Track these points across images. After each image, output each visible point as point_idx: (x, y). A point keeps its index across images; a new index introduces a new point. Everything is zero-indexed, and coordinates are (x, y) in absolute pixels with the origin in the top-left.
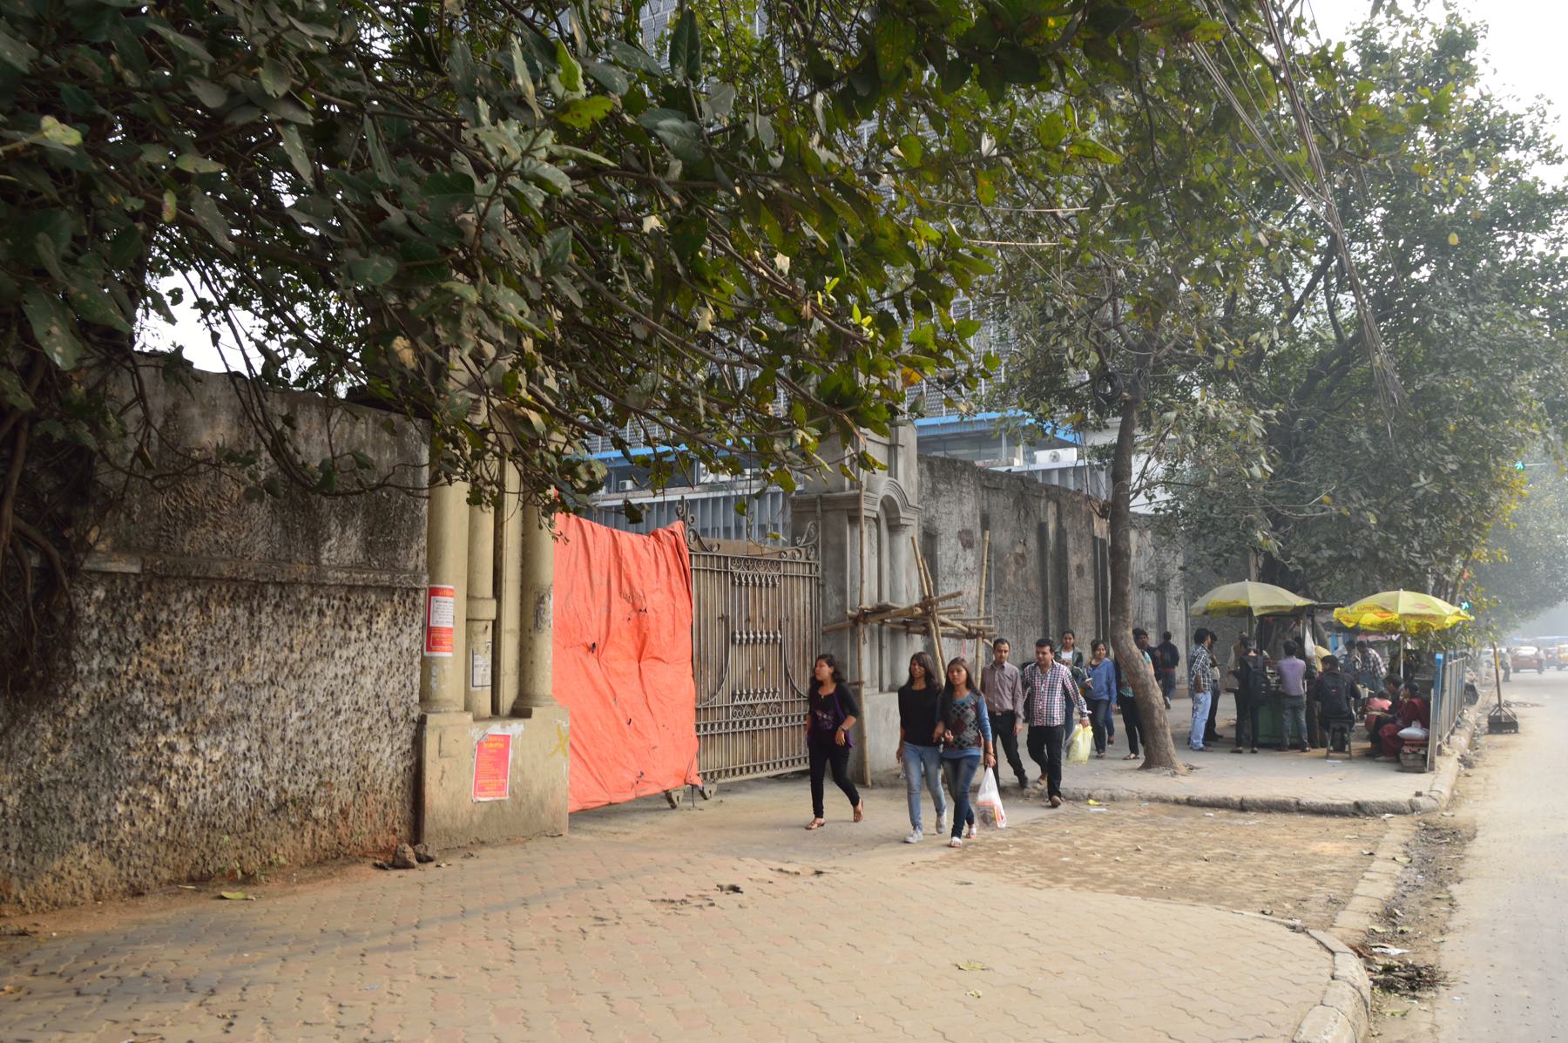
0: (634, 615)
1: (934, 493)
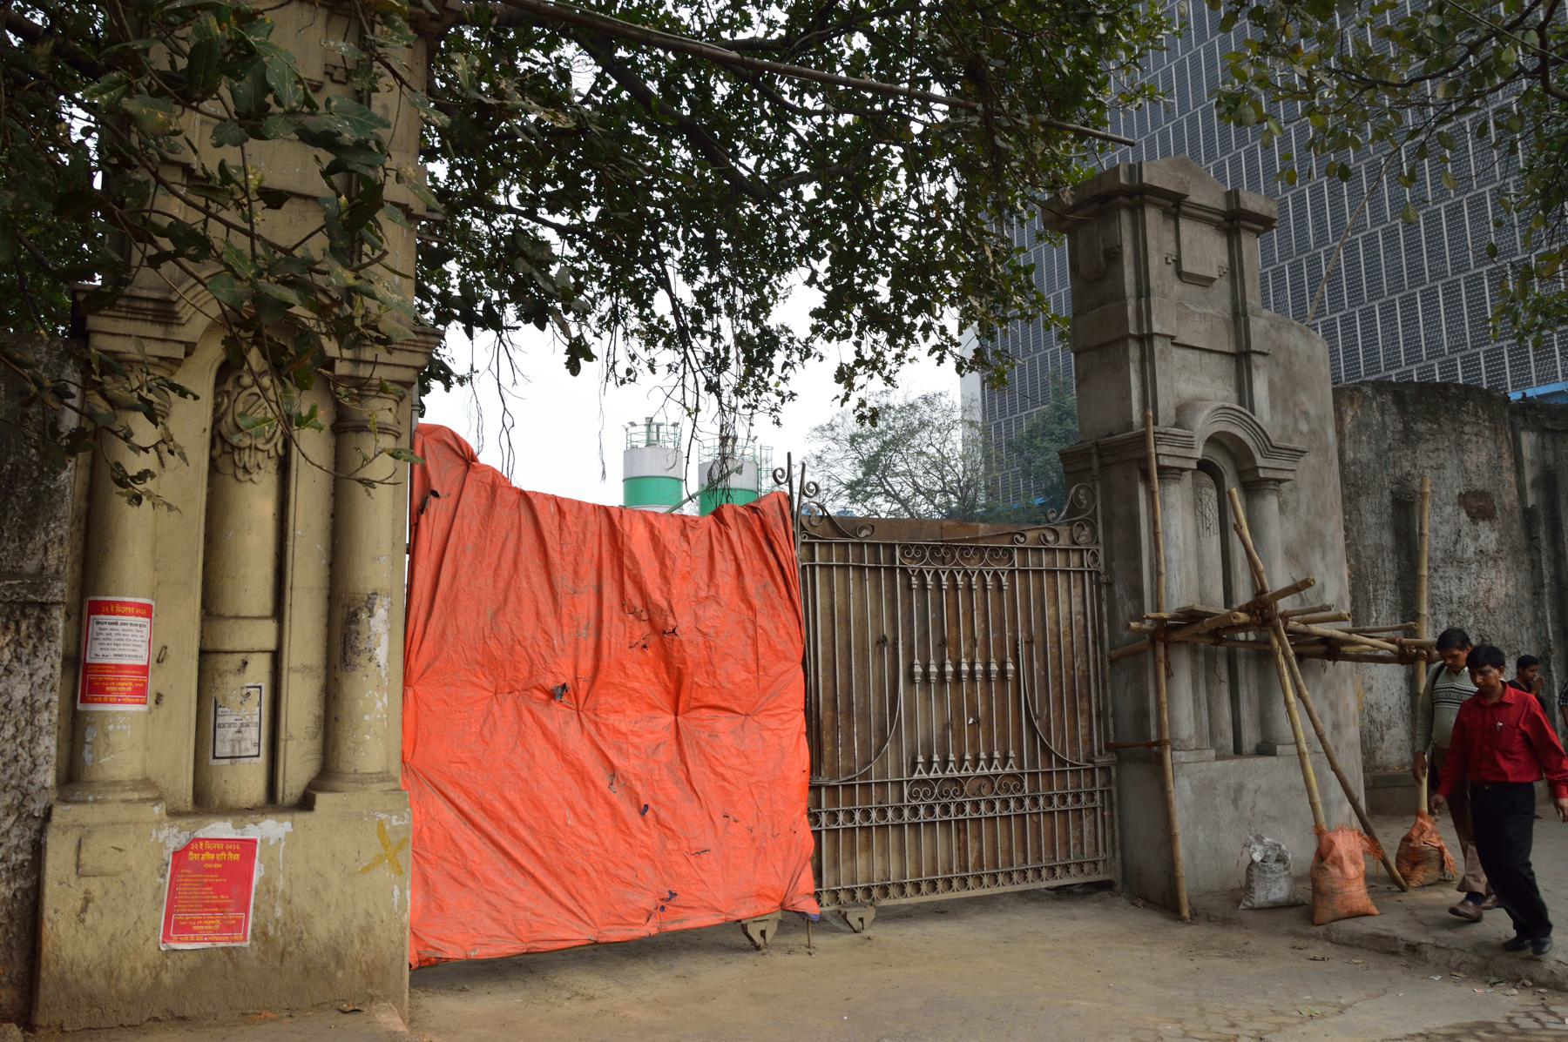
0: (654, 639)
1: (1409, 438)
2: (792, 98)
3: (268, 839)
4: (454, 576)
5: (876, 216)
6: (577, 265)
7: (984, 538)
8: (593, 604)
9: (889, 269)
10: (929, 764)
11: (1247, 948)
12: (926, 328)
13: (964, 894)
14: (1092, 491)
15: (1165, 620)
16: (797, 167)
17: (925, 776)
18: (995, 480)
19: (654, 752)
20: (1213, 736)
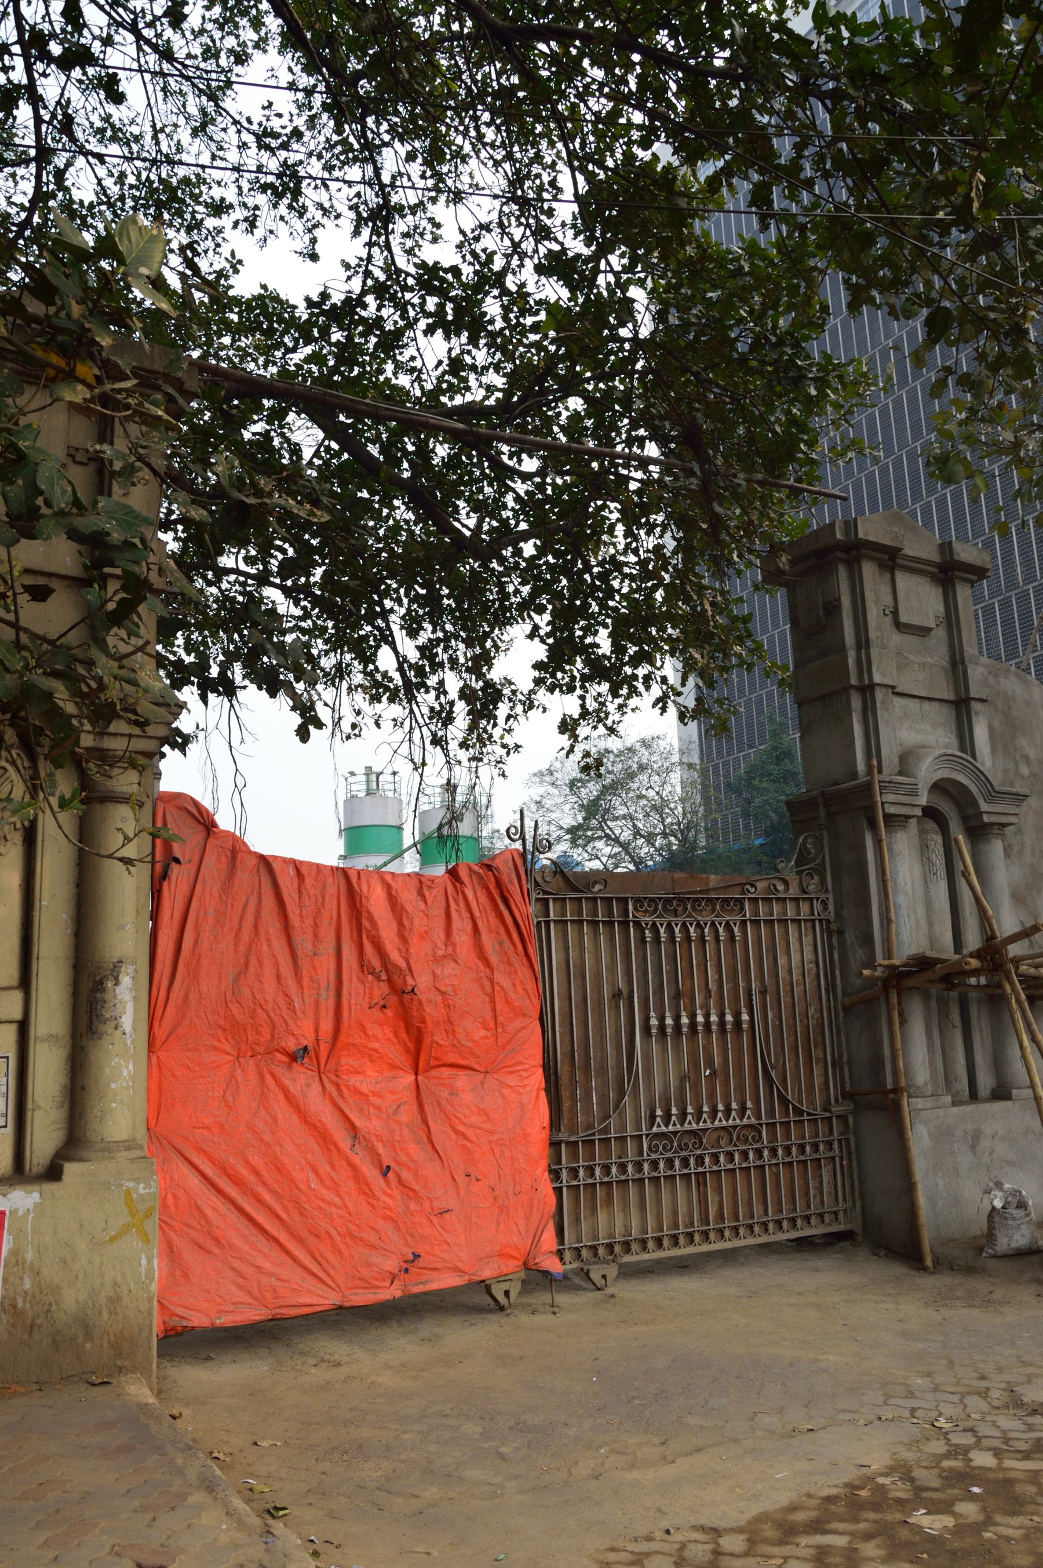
0: (394, 999)
2: (510, 458)
3: (17, 1210)
4: (196, 941)
5: (596, 570)
6: (303, 624)
7: (715, 889)
8: (332, 965)
9: (609, 621)
10: (667, 1118)
11: (991, 1297)
12: (647, 678)
13: (706, 1248)
14: (819, 840)
15: (897, 967)
16: (517, 525)
17: (663, 1129)
18: (715, 822)
19: (395, 1114)
20: (949, 1080)
